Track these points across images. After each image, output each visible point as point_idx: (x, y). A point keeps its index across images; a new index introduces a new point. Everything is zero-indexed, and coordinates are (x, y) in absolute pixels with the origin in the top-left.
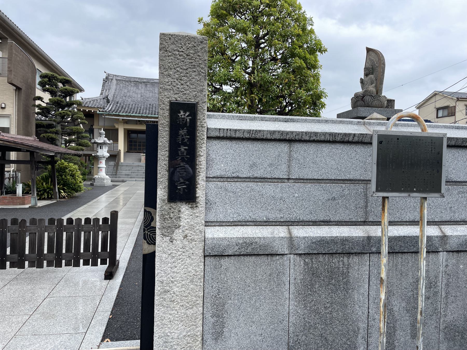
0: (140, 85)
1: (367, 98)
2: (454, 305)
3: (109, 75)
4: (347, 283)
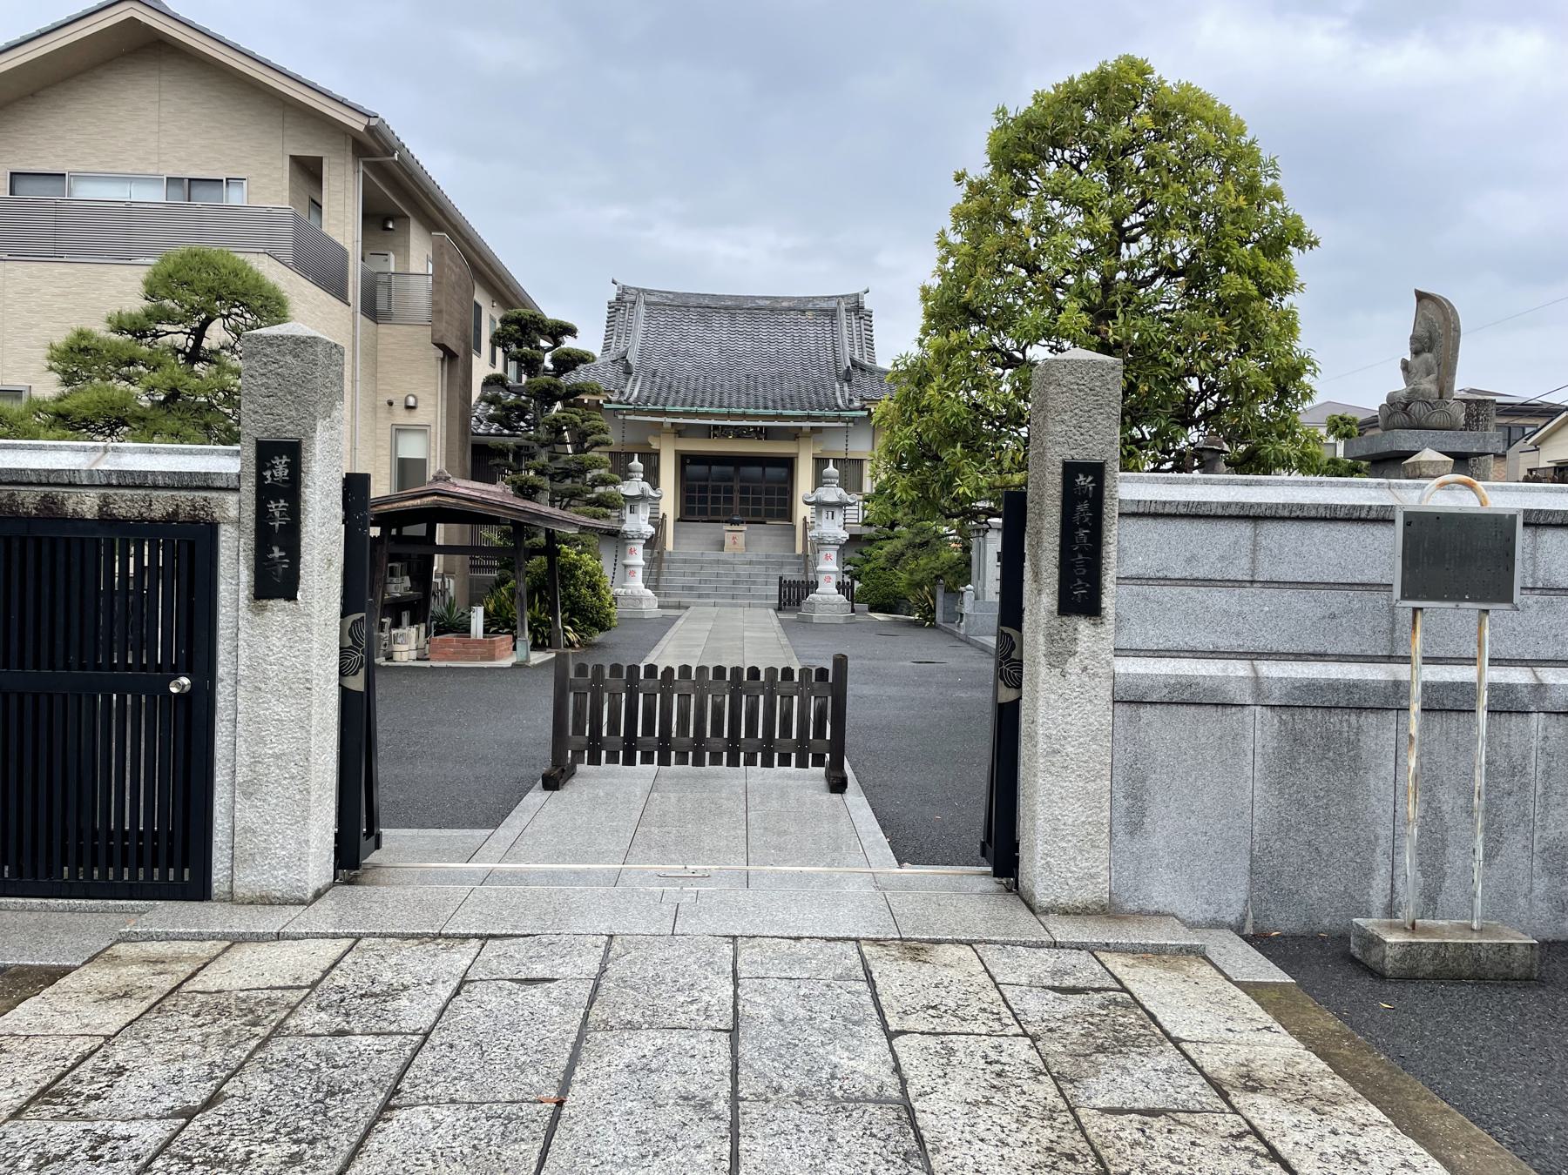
0: (716, 317)
1: (1416, 408)
2: (1561, 810)
4: (1355, 759)
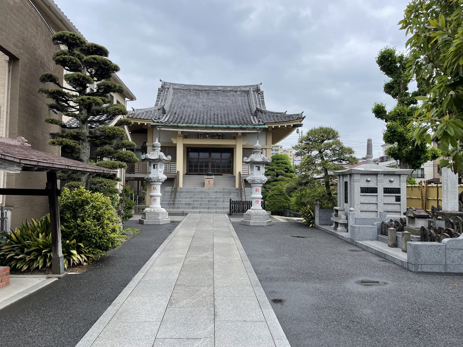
3: (165, 84)
